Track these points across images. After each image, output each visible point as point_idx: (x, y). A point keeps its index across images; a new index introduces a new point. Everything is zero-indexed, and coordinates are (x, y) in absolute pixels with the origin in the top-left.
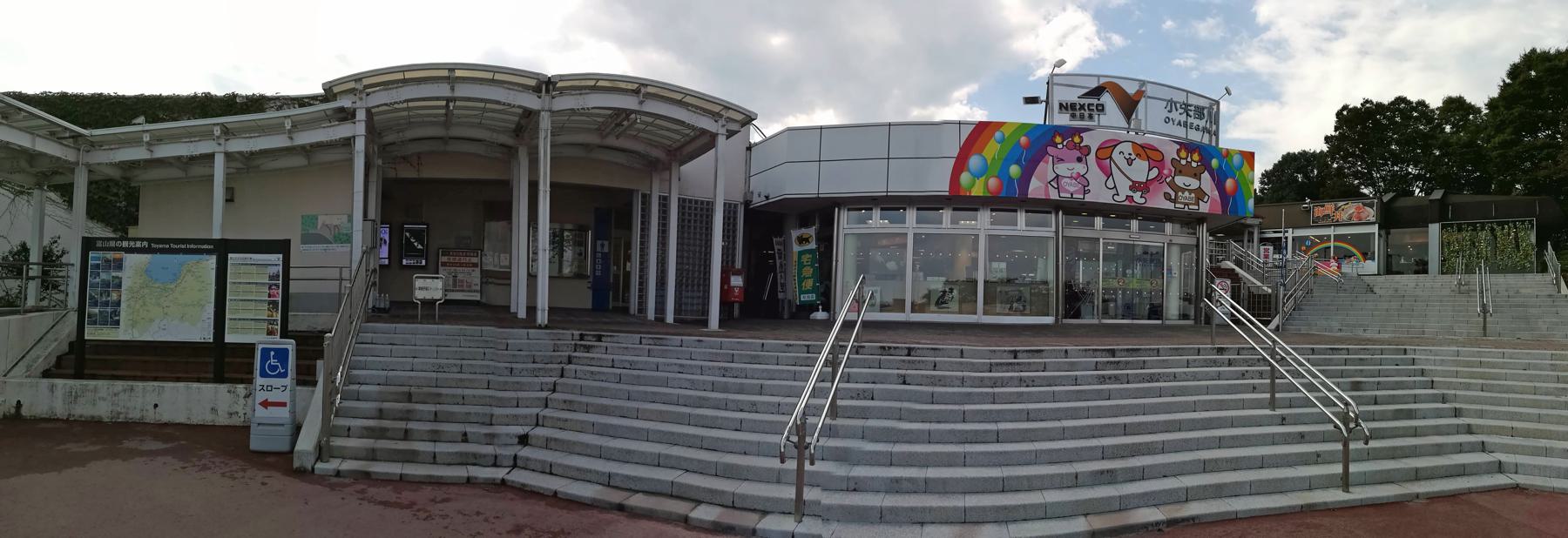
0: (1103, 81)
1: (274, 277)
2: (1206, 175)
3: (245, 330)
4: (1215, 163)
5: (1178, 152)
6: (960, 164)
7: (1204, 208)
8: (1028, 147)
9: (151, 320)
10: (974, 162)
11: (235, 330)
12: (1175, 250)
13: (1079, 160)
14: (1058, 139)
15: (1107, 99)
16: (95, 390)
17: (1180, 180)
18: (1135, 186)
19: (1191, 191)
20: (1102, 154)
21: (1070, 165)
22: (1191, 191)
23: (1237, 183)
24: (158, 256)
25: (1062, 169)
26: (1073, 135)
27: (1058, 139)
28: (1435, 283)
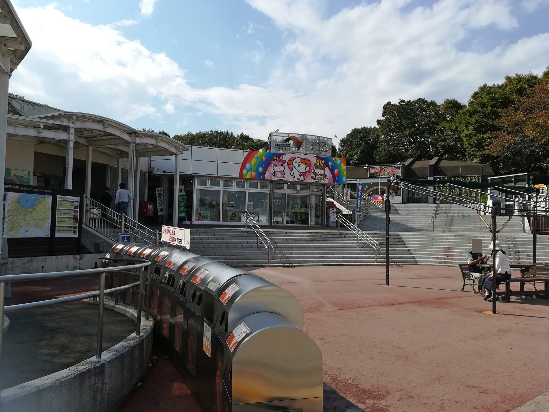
0: (290, 135)
1: (76, 207)
2: (327, 169)
3: (64, 231)
4: (330, 163)
5: (316, 160)
6: (243, 167)
7: (326, 181)
8: (266, 160)
9: (21, 227)
10: (248, 166)
11: (59, 231)
12: (314, 197)
13: (282, 165)
14: (275, 158)
15: (291, 142)
16: (14, 263)
17: (317, 171)
18: (301, 174)
19: (321, 175)
20: (289, 163)
21: (279, 167)
22: (321, 175)
23: (339, 171)
24: (24, 194)
25: (276, 169)
26: (280, 156)
27: (275, 158)
28: (428, 209)
